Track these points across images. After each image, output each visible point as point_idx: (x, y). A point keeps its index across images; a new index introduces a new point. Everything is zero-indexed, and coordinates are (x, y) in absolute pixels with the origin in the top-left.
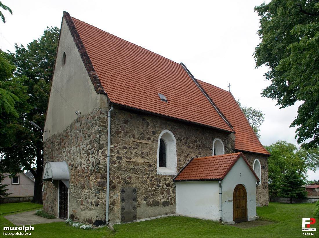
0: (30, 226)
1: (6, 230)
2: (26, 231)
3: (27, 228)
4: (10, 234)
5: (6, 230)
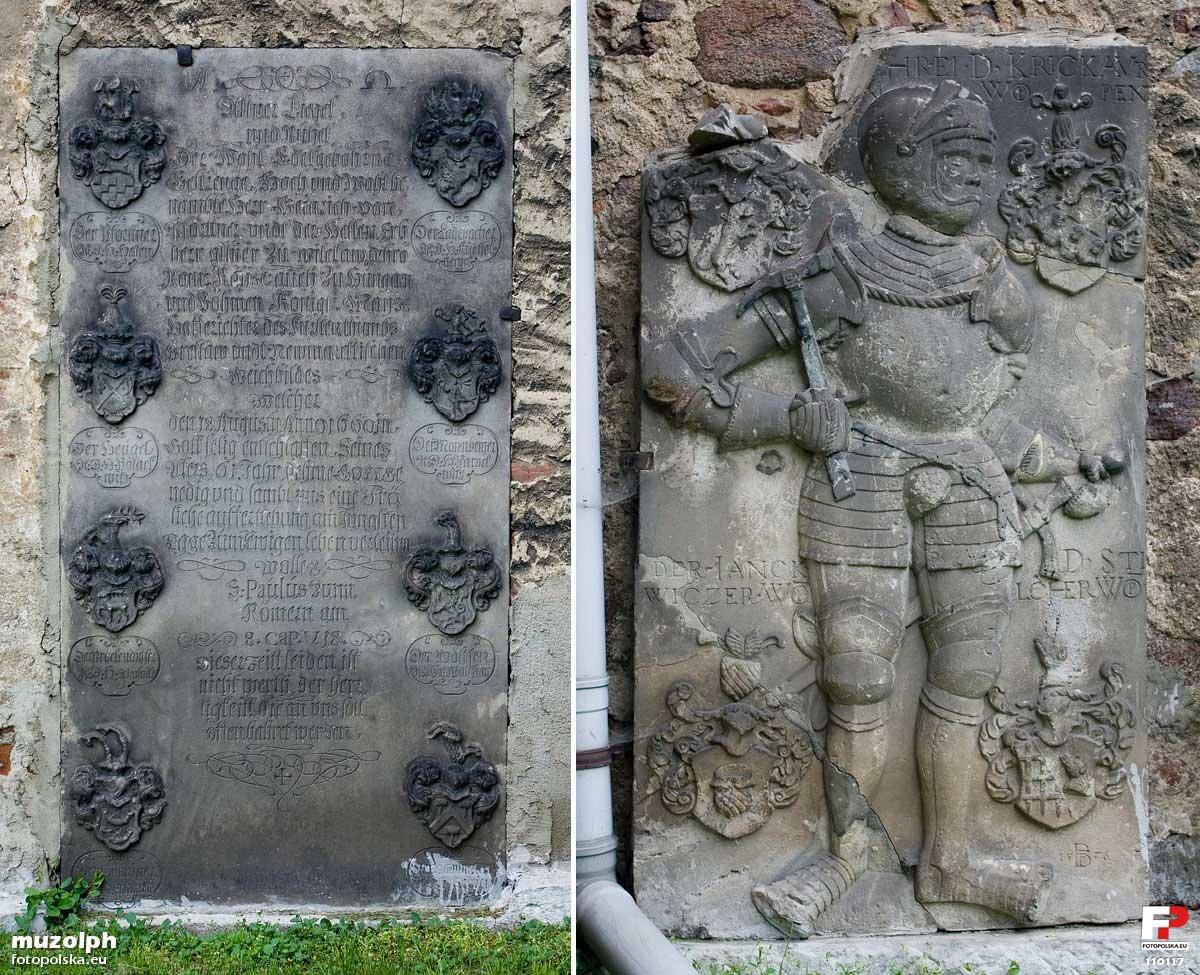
0: (105, 934)
1: (22, 946)
2: (88, 951)
3: (93, 942)
4: (36, 960)
5: (22, 946)
